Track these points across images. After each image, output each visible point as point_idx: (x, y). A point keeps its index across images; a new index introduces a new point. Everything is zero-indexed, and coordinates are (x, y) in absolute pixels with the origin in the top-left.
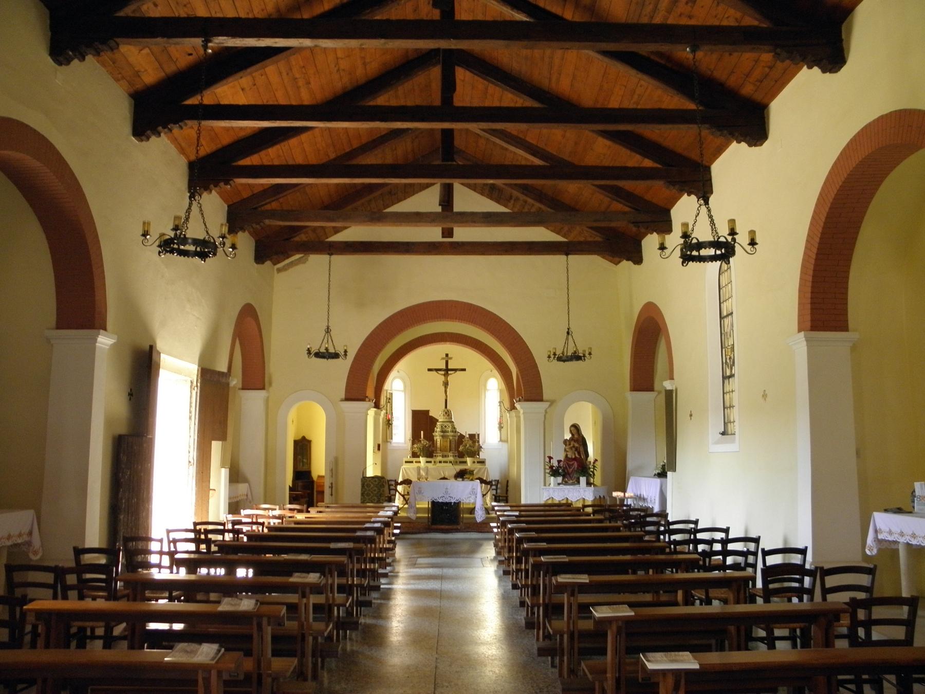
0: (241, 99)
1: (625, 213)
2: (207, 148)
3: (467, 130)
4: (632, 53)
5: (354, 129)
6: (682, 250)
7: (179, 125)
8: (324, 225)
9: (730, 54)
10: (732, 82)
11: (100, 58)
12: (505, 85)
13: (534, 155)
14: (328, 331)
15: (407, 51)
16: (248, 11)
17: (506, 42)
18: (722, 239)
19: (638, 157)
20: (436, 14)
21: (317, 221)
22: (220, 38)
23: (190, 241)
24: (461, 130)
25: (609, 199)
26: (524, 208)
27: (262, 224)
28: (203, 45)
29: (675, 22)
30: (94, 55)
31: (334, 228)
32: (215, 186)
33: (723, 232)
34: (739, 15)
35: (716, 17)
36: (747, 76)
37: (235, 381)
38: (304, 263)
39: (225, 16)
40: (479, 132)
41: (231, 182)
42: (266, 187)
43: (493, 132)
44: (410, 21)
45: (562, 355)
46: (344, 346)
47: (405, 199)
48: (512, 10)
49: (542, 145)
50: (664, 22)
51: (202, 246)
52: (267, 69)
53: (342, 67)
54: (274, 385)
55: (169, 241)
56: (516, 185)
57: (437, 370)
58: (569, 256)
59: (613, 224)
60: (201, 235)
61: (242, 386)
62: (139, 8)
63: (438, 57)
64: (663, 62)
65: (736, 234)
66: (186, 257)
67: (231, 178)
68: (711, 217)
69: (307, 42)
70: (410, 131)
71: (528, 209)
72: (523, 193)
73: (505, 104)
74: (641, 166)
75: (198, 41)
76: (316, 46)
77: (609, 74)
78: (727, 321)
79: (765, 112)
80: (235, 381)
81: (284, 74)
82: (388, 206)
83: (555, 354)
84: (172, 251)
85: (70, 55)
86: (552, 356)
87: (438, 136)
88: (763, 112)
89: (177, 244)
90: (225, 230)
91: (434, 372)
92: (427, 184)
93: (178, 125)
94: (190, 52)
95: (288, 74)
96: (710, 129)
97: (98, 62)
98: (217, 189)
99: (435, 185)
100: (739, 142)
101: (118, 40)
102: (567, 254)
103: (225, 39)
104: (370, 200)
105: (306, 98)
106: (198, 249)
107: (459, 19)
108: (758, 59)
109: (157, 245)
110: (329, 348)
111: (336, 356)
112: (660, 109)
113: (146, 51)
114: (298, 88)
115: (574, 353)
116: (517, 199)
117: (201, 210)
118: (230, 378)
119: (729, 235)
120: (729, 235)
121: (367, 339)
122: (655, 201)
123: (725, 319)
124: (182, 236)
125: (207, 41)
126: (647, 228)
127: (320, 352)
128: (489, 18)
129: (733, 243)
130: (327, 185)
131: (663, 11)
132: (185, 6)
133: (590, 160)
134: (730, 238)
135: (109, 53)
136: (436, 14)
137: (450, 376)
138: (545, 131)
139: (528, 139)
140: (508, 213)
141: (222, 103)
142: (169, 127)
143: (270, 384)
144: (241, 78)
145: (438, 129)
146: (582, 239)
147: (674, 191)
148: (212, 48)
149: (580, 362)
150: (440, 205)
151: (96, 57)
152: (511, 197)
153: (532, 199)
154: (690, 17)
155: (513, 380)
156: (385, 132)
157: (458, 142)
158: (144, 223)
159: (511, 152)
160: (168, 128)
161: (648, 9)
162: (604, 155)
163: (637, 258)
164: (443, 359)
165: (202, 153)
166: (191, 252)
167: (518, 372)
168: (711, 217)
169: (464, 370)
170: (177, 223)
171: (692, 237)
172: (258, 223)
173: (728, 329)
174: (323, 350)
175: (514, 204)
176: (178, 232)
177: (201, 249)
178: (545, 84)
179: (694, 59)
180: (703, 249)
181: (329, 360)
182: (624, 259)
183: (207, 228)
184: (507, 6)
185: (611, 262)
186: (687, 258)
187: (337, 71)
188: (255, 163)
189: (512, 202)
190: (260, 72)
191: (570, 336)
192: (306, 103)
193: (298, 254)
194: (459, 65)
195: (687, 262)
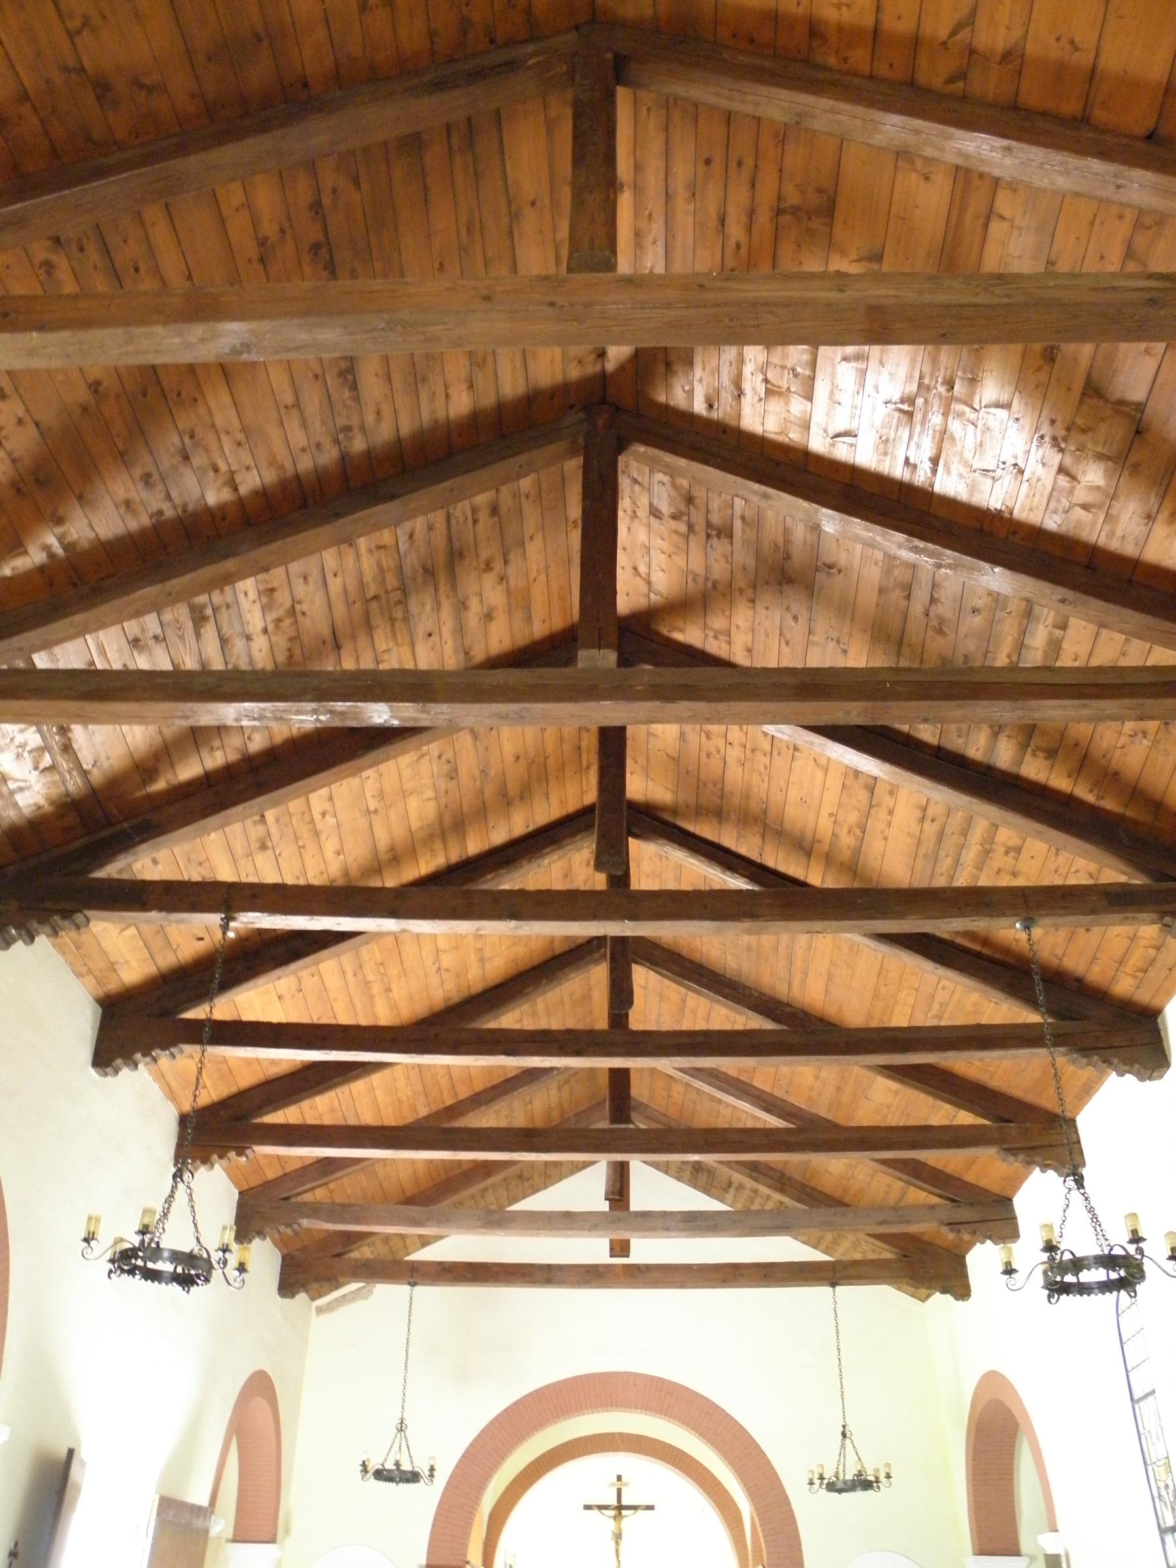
0: (276, 1014)
1: (933, 1207)
2: (212, 1092)
3: (653, 1071)
4: (926, 935)
5: (460, 1067)
6: (1045, 1273)
7: (171, 1053)
8: (403, 1232)
9: (1088, 930)
10: (1096, 975)
11: (58, 941)
12: (715, 993)
13: (767, 1110)
14: (401, 1428)
15: (552, 940)
16: (298, 874)
17: (716, 924)
18: (1118, 1251)
19: (948, 1107)
20: (599, 881)
21: (391, 1224)
22: (251, 914)
23: (166, 1254)
24: (642, 1070)
25: (901, 1184)
26: (752, 1202)
27: (296, 1227)
28: (221, 925)
29: (990, 884)
30: (48, 936)
31: (421, 1236)
32: (221, 1157)
33: (1119, 1242)
34: (1092, 867)
35: (1056, 871)
36: (1121, 962)
37: (221, 1525)
38: (366, 1298)
39: (262, 881)
40: (672, 1072)
41: (248, 1152)
42: (307, 1163)
43: (697, 1072)
44: (558, 892)
45: (834, 1479)
46: (430, 1458)
47: (545, 1187)
48: (723, 872)
49: (779, 1093)
50: (973, 884)
51: (186, 1265)
52: (321, 966)
53: (445, 965)
54: (293, 1532)
55: (130, 1253)
56: (738, 1163)
57: (601, 1508)
58: (838, 1288)
59: (912, 1229)
60: (186, 1245)
61: (235, 1535)
62: (130, 866)
63: (603, 950)
64: (977, 948)
65: (1142, 1239)
66: (156, 1283)
67: (246, 1145)
68: (1091, 1210)
69: (389, 925)
70: (556, 1072)
71: (761, 1205)
72: (751, 1177)
73: (715, 1026)
74: (954, 1123)
75: (215, 919)
76: (404, 931)
77: (888, 971)
78: (1145, 1407)
79: (1159, 1020)
80: (221, 1525)
81: (350, 974)
82: (516, 1200)
83: (821, 1478)
84: (131, 1272)
85: (12, 935)
86: (817, 1482)
87: (604, 1081)
88: (1156, 1024)
89: (142, 1258)
90: (229, 1237)
91: (596, 1512)
92: (584, 1162)
93: (168, 1052)
94: (200, 936)
95: (355, 975)
96: (1067, 1055)
97: (54, 946)
98: (224, 1162)
99: (598, 1164)
100: (1121, 1074)
101: (89, 913)
102: (833, 1285)
103: (257, 917)
104: (486, 1189)
105: (384, 1016)
106: (179, 1270)
107: (637, 888)
108: (1135, 935)
109: (108, 1259)
110: (402, 1462)
111: (413, 1477)
112: (979, 1026)
113: (132, 931)
114: (372, 997)
115: (857, 1476)
116: (741, 1187)
117: (191, 1200)
118: (213, 1517)
119: (1131, 1242)
120: (1131, 1242)
121: (473, 1445)
122: (984, 1183)
123: (1141, 1404)
124: (153, 1245)
125: (228, 919)
126: (974, 1233)
127: (385, 1470)
128: (686, 886)
129: (1139, 1257)
130: (413, 1162)
131: (970, 868)
132: (200, 864)
133: (865, 1116)
134: (1131, 1249)
135: (73, 933)
136: (599, 881)
137: (625, 1519)
138: (785, 1070)
139: (757, 1084)
140: (728, 1212)
141: (245, 1018)
142: (153, 1054)
143: (287, 1531)
144: (279, 978)
145: (601, 1069)
146: (858, 1256)
147: (1014, 1164)
148: (236, 931)
149: (870, 1492)
150: (606, 1199)
151: (52, 939)
152: (730, 1184)
153: (769, 1187)
154: (1014, 874)
155: (743, 1530)
156: (514, 1073)
157: (638, 1090)
158: (90, 1219)
159: (728, 1105)
160: (152, 1056)
161: (946, 864)
162: (889, 1107)
163: (961, 1290)
164: (612, 1485)
165: (204, 1099)
166: (164, 1275)
167: (755, 1515)
168: (1091, 1210)
169: (651, 1508)
170: (146, 1221)
171: (1062, 1249)
172: (288, 1225)
173: (1149, 1424)
174: (390, 1466)
175: (735, 1196)
176: (147, 1238)
177: (183, 1270)
178: (781, 991)
179: (1029, 940)
180: (1085, 1271)
181: (401, 1485)
182: (936, 1289)
183: (197, 1232)
184: (715, 867)
185: (912, 1296)
186: (1057, 1289)
187: (437, 972)
188: (292, 1121)
189: (732, 1191)
190: (309, 971)
191: (848, 1441)
192: (383, 1022)
193: (355, 1282)
194: (636, 963)
195: (1056, 1296)
